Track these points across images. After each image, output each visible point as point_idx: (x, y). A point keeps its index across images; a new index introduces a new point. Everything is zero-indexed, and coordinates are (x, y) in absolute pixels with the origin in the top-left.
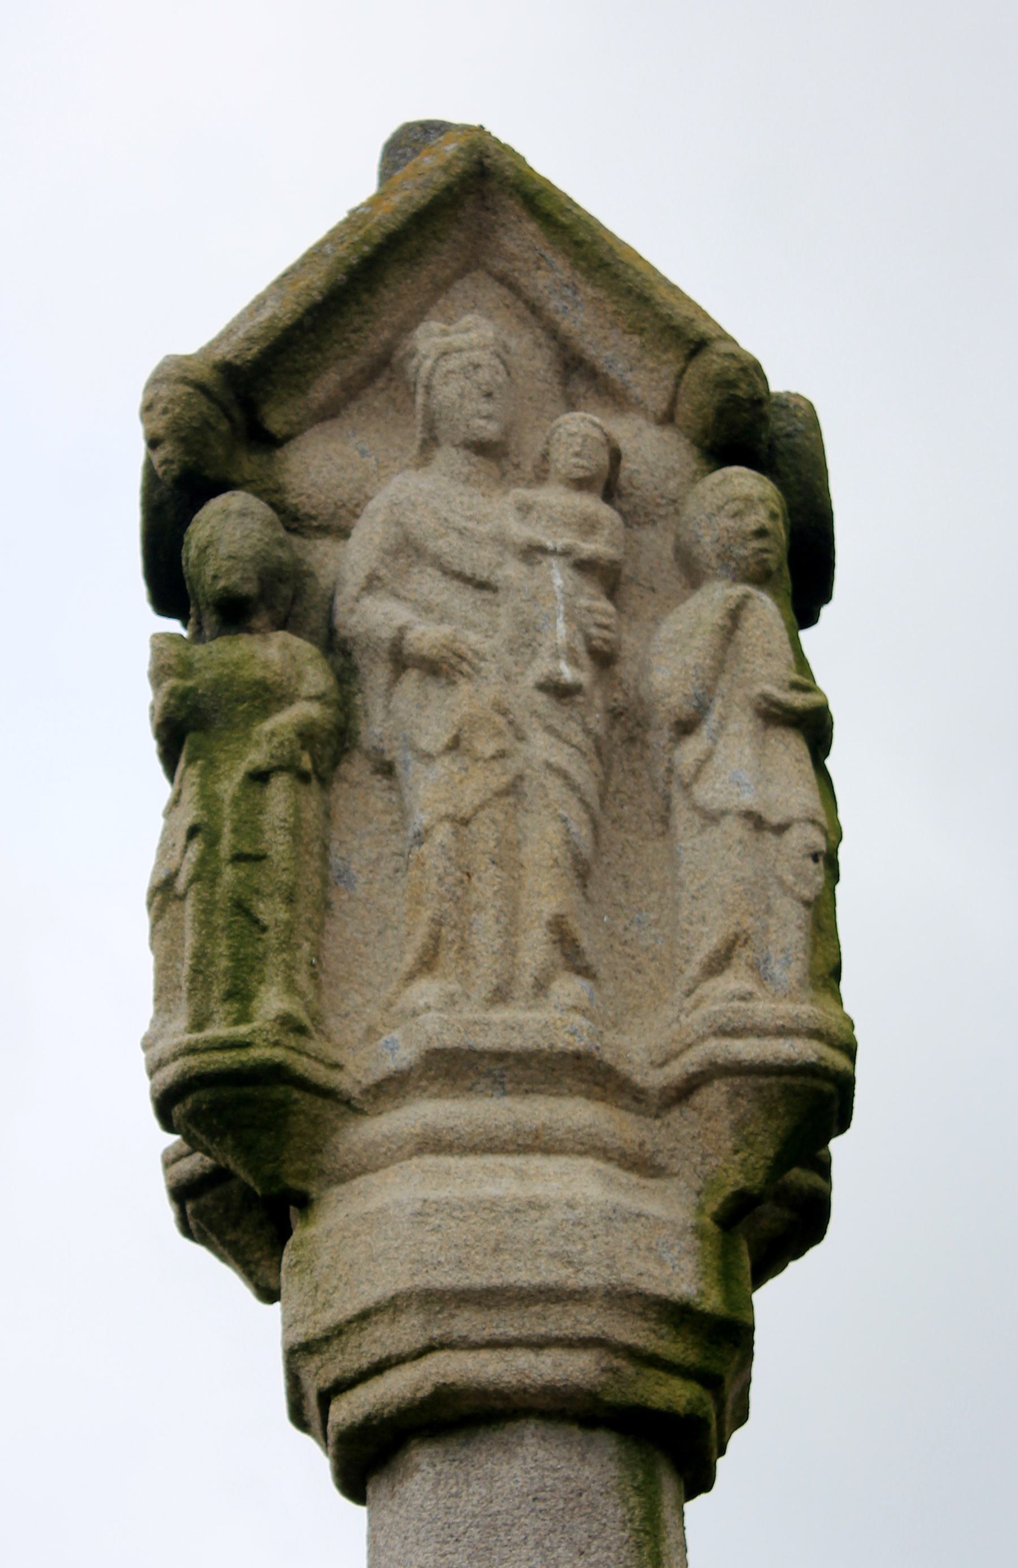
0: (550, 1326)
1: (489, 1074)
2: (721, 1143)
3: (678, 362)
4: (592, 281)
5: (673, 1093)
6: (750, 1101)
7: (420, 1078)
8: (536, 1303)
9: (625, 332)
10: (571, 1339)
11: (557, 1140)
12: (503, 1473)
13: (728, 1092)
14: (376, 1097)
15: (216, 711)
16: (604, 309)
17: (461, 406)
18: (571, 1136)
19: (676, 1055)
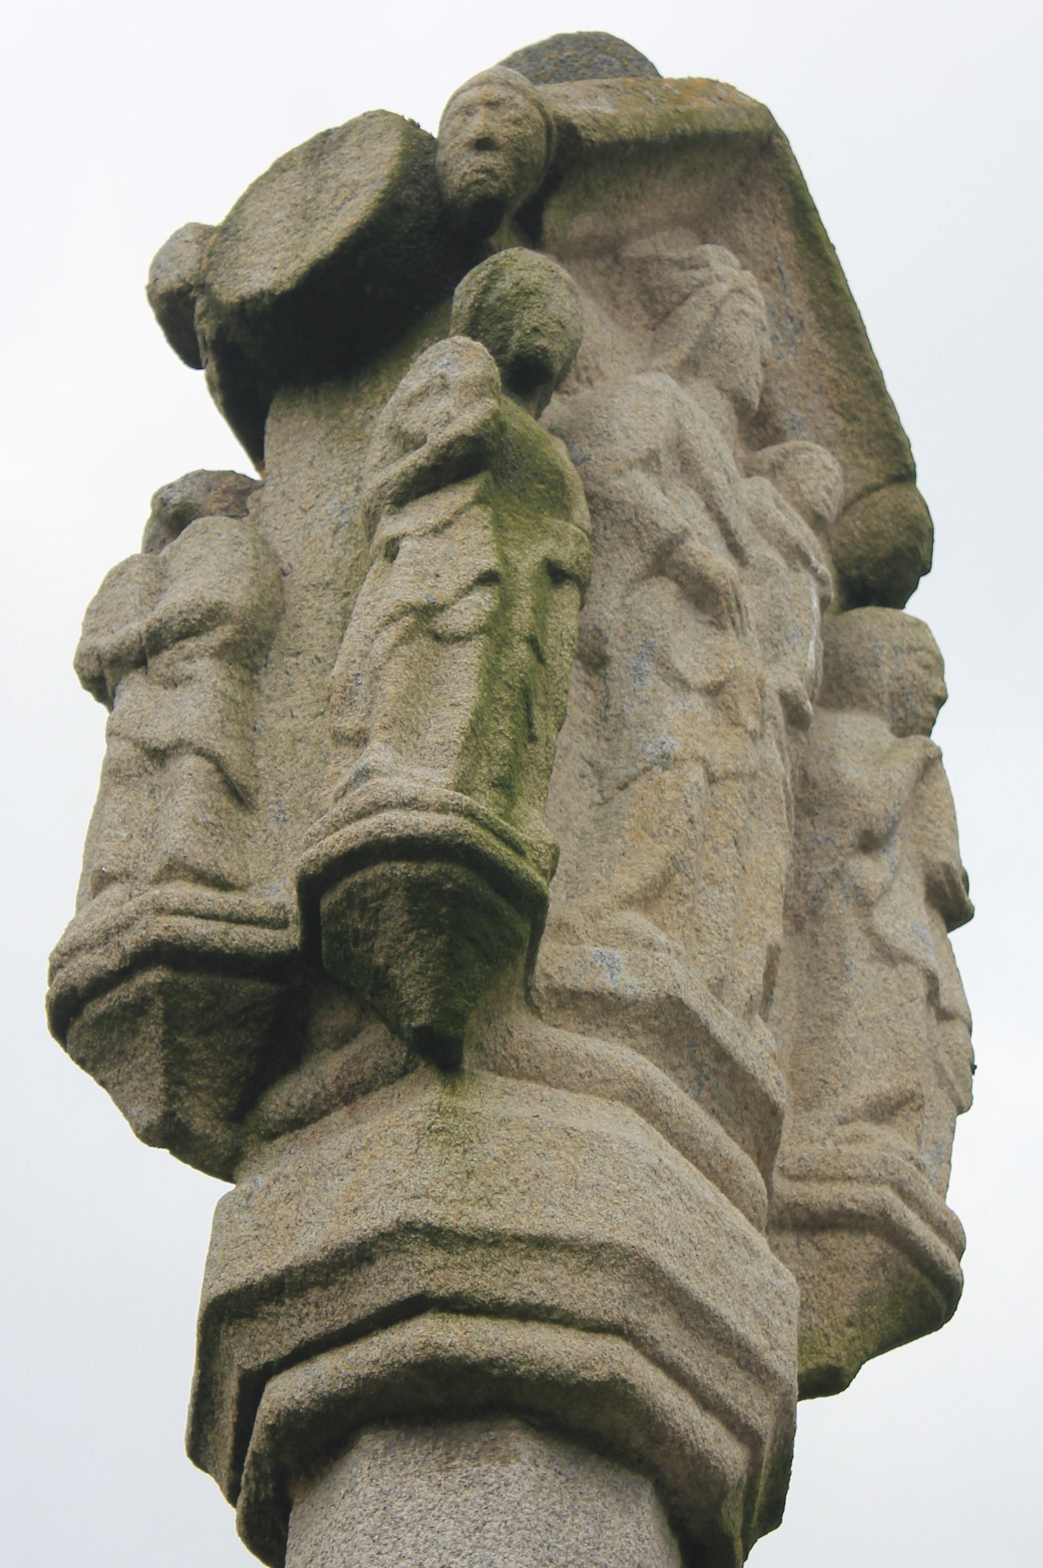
0: (728, 1390)
1: (699, 1066)
2: (836, 1304)
3: (878, 477)
4: (825, 333)
5: (804, 1216)
6: (887, 1280)
7: (637, 1019)
8: (728, 1355)
9: (831, 407)
10: (739, 1420)
11: (739, 1187)
12: (613, 1523)
13: (878, 1255)
14: (561, 1006)
15: (514, 469)
16: (823, 369)
17: (748, 355)
18: (751, 1192)
19: (822, 1179)
